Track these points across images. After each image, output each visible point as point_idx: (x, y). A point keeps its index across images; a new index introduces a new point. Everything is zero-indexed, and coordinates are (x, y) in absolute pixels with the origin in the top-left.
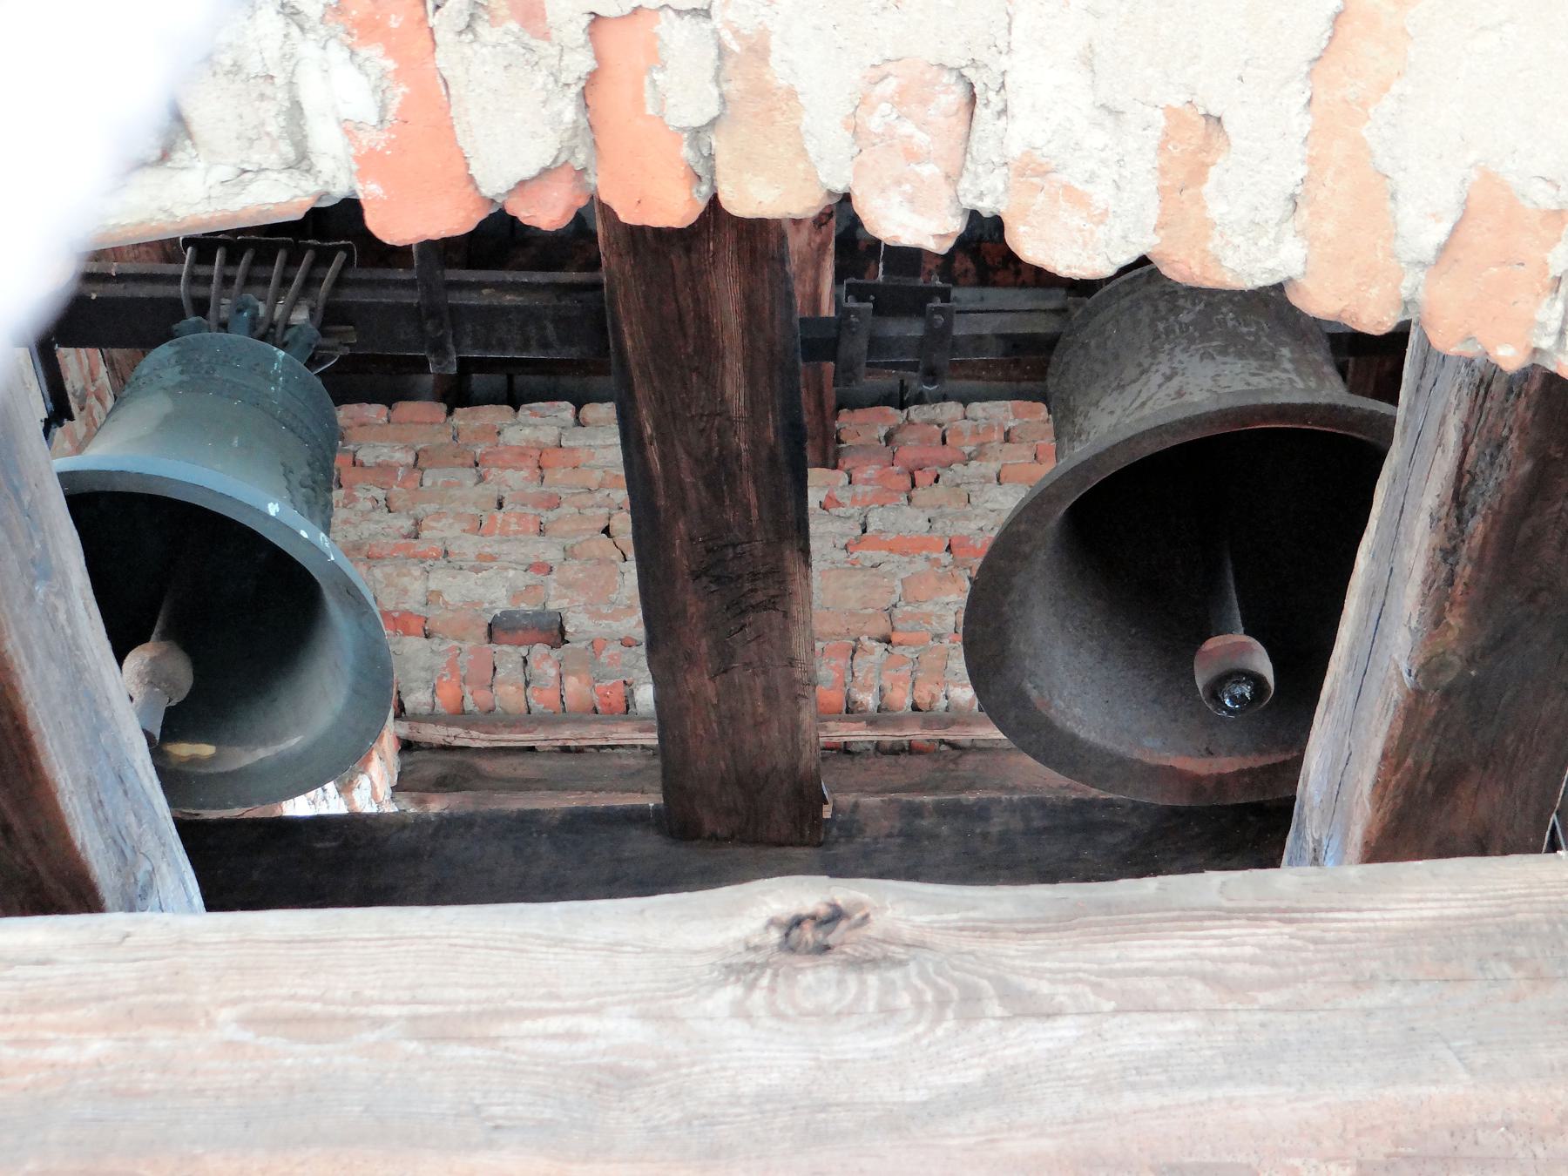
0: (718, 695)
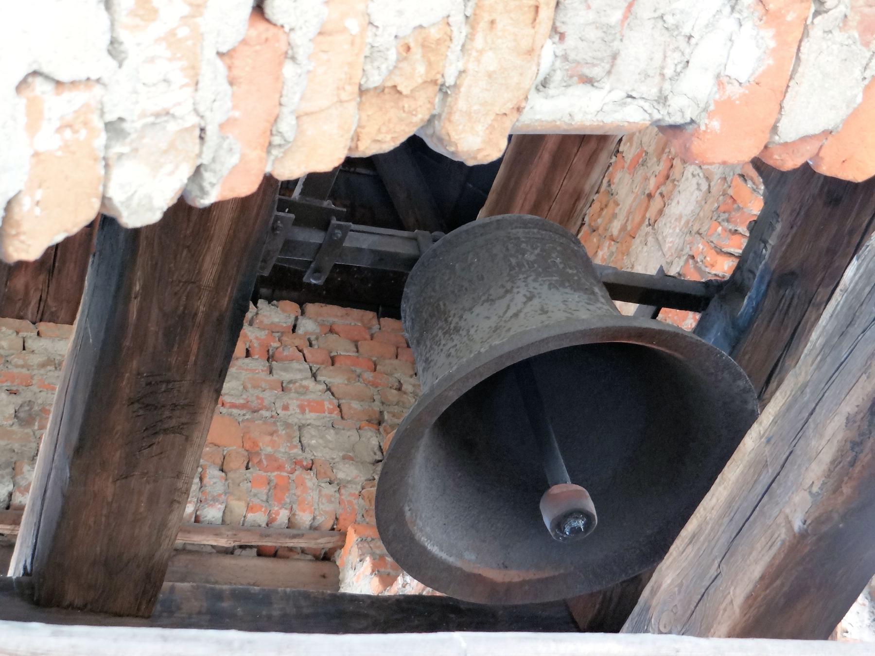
0: (114, 495)
